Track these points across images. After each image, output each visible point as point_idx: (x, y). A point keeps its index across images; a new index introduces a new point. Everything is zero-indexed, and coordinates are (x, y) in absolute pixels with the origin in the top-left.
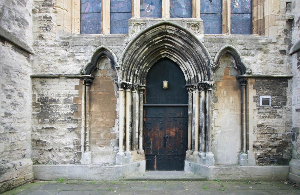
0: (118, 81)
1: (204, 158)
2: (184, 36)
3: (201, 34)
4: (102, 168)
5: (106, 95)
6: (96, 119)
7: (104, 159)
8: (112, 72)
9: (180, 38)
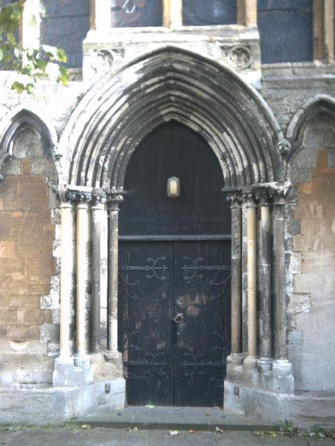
0: (59, 186)
1: (268, 373)
2: (214, 76)
3: (254, 69)
4: (21, 395)
5: (31, 218)
6: (8, 277)
7: (25, 372)
8: (45, 164)
9: (203, 80)
